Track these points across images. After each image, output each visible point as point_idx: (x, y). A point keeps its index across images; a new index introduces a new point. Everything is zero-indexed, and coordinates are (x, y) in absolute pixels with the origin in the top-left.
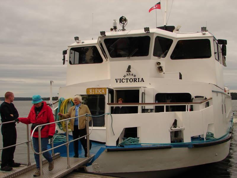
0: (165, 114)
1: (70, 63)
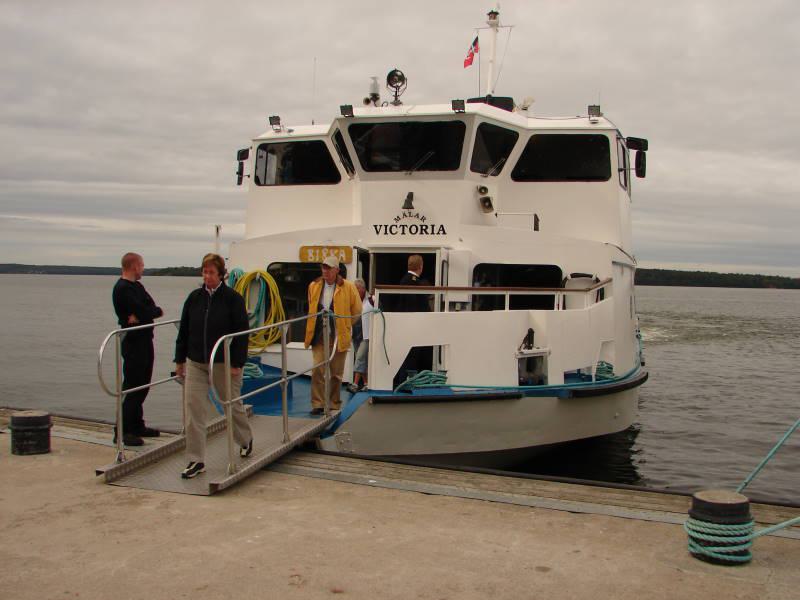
0: (507, 315)
1: (257, 181)
